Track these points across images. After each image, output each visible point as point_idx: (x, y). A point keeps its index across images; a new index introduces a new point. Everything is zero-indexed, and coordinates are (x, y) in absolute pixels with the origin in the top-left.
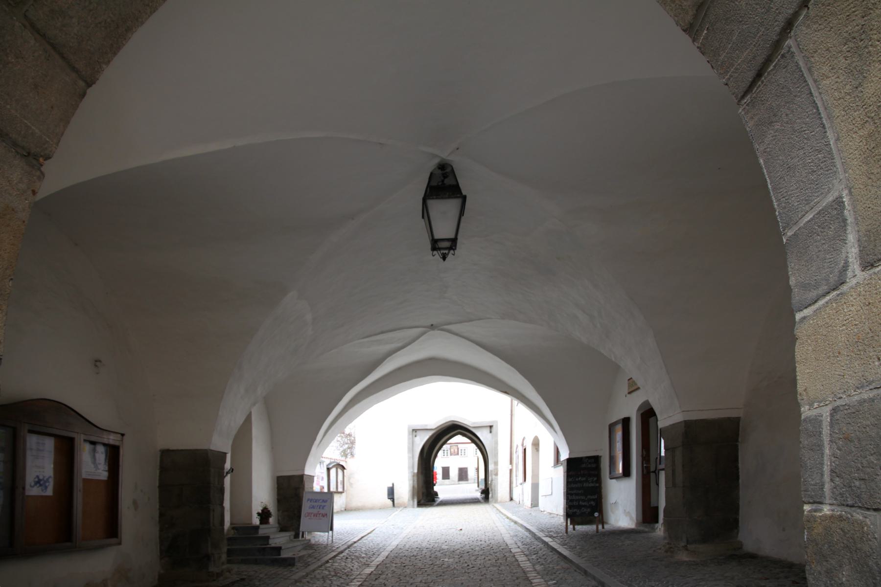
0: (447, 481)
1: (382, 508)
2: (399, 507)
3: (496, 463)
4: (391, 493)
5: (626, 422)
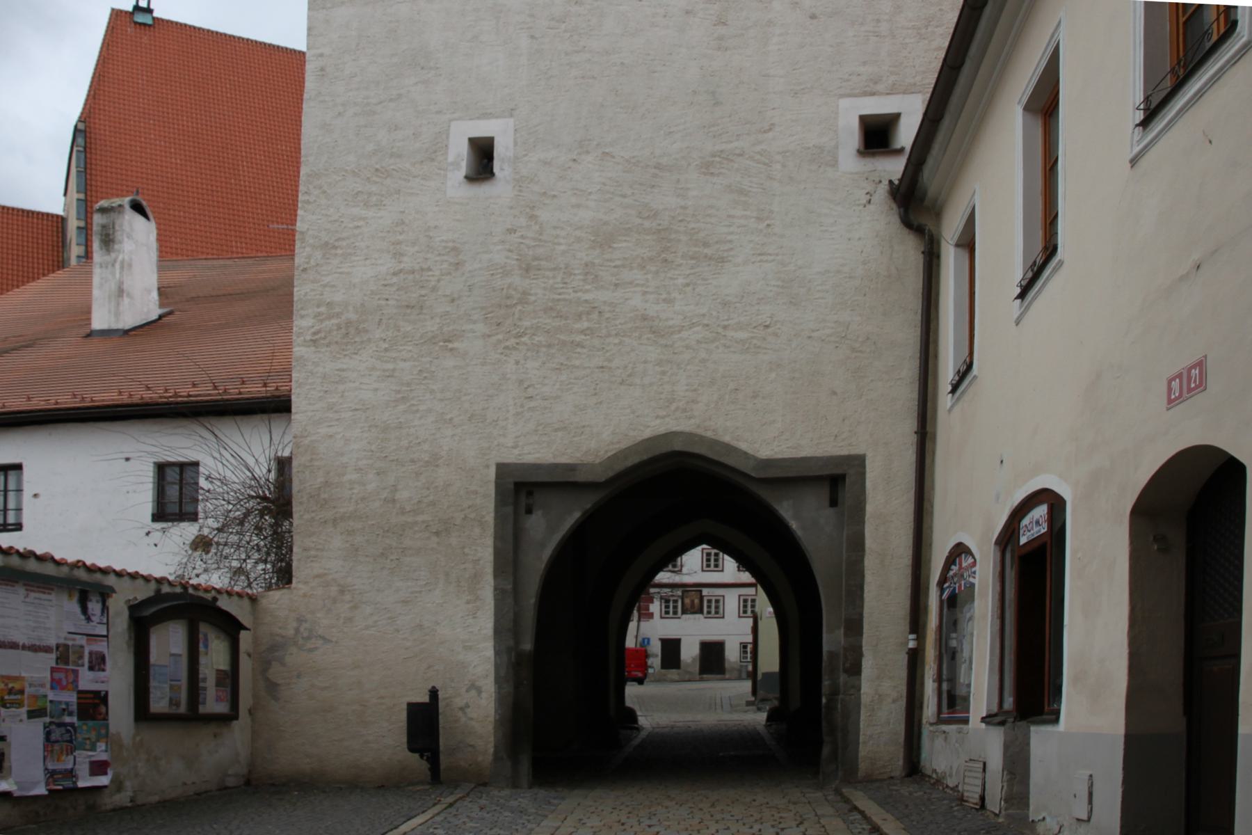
0: (673, 674)
2: (454, 784)
3: (854, 626)
4: (424, 721)
5: (1035, 570)
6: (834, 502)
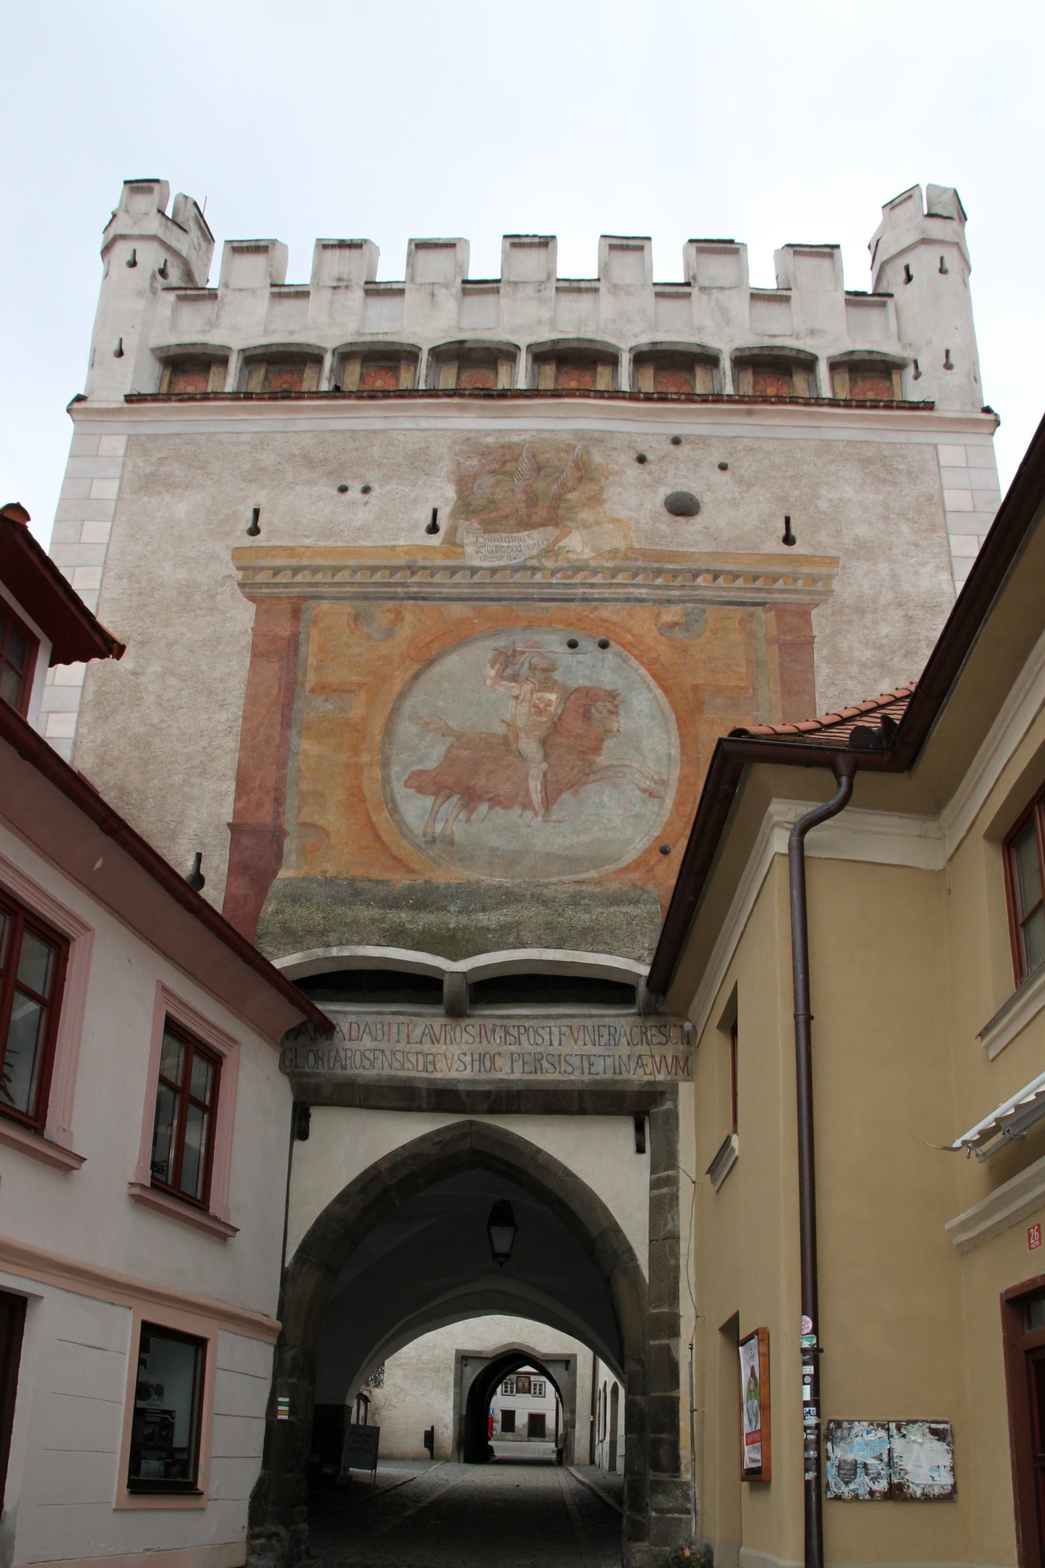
1: (417, 1459)
4: (430, 1437)
6: (567, 1369)
